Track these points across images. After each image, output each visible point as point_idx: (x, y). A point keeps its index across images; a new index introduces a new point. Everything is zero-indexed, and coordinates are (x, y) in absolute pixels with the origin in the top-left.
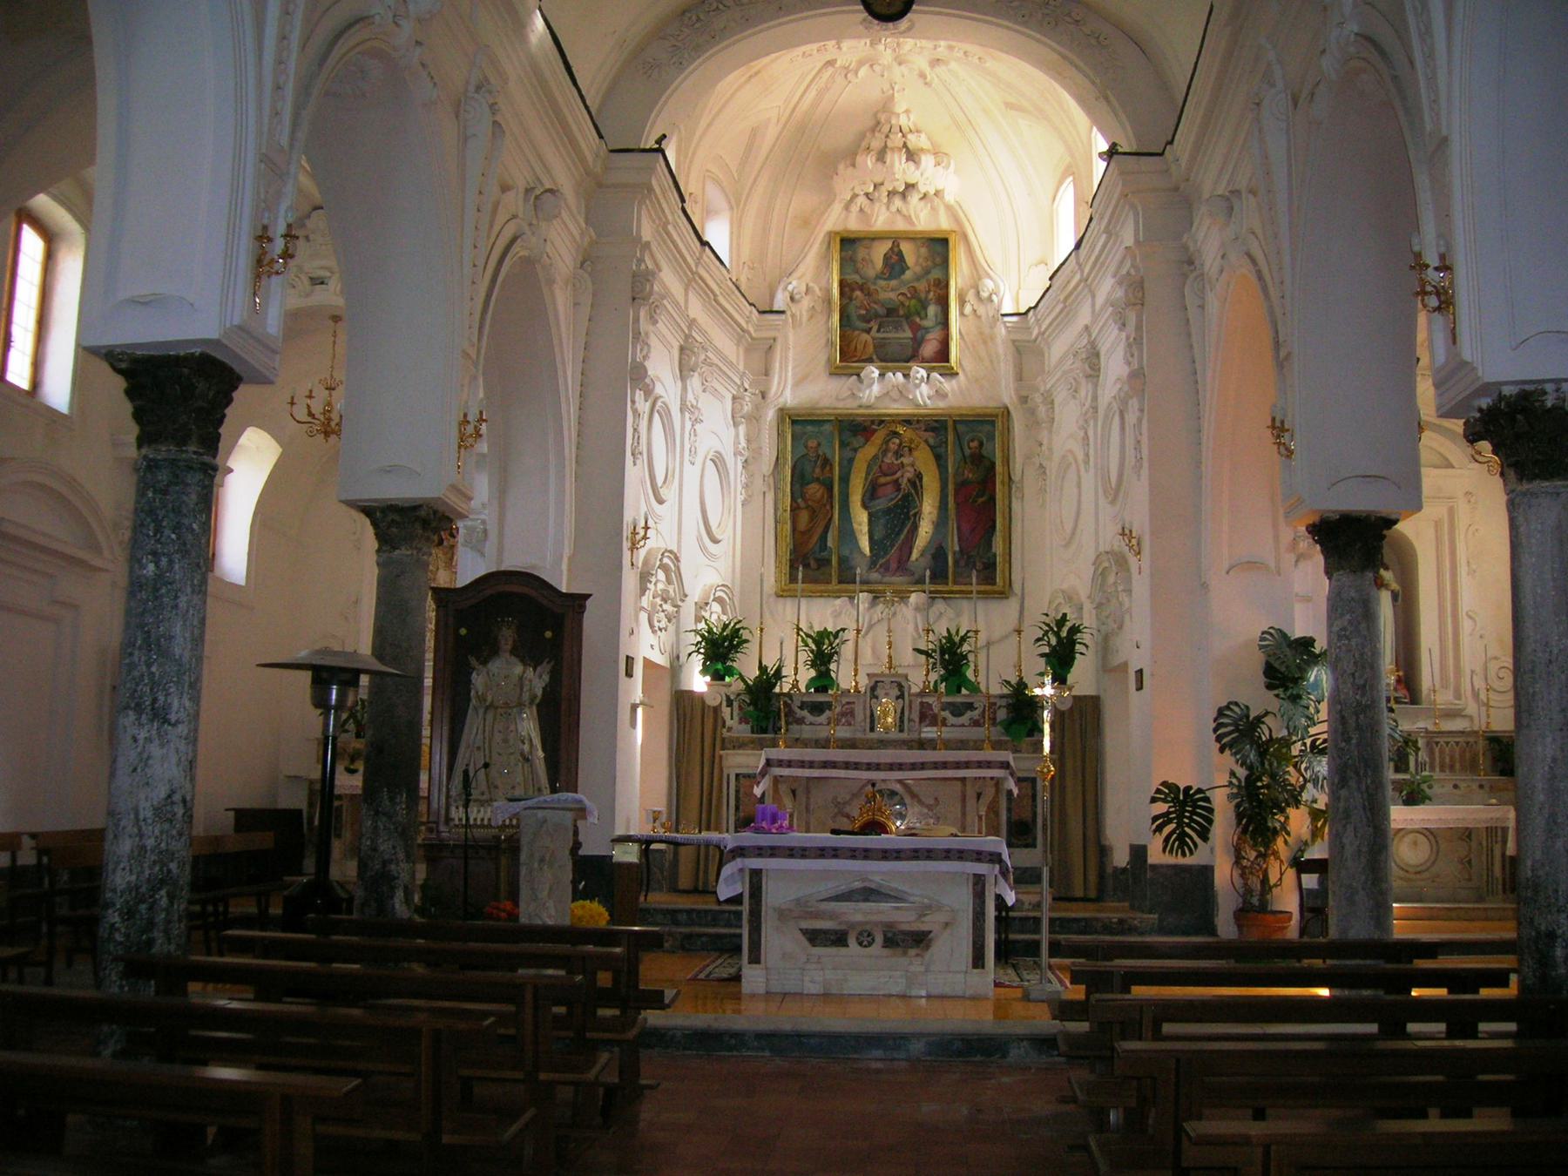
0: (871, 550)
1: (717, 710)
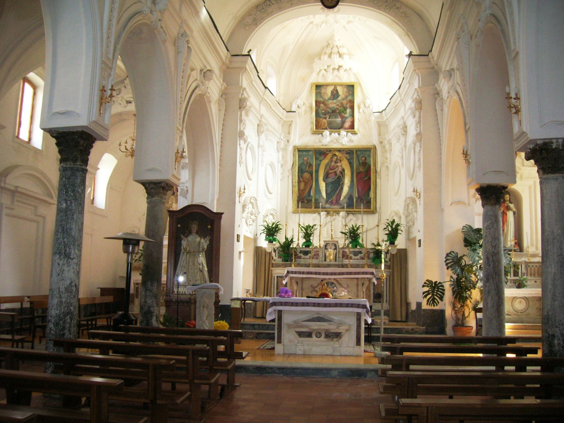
0: (326, 196)
1: (270, 253)
